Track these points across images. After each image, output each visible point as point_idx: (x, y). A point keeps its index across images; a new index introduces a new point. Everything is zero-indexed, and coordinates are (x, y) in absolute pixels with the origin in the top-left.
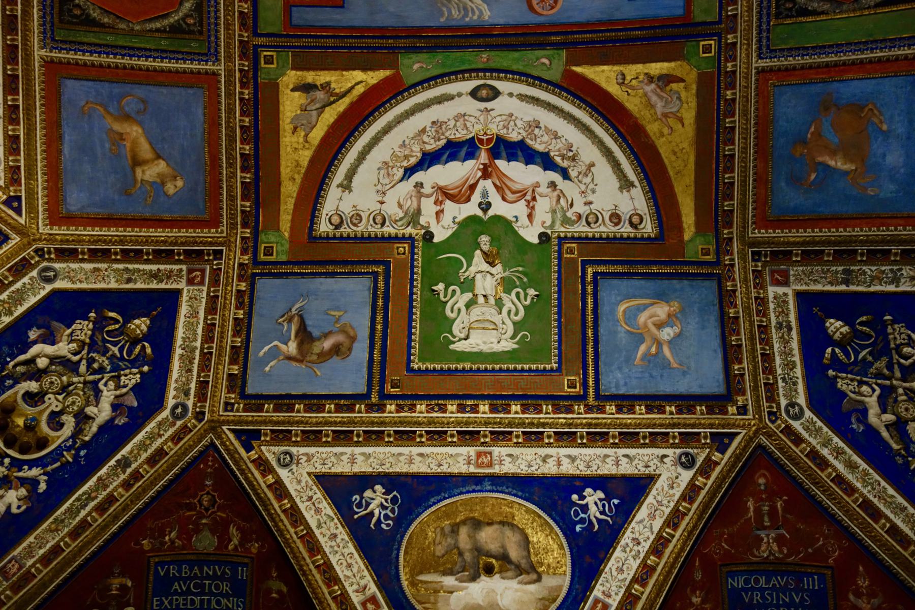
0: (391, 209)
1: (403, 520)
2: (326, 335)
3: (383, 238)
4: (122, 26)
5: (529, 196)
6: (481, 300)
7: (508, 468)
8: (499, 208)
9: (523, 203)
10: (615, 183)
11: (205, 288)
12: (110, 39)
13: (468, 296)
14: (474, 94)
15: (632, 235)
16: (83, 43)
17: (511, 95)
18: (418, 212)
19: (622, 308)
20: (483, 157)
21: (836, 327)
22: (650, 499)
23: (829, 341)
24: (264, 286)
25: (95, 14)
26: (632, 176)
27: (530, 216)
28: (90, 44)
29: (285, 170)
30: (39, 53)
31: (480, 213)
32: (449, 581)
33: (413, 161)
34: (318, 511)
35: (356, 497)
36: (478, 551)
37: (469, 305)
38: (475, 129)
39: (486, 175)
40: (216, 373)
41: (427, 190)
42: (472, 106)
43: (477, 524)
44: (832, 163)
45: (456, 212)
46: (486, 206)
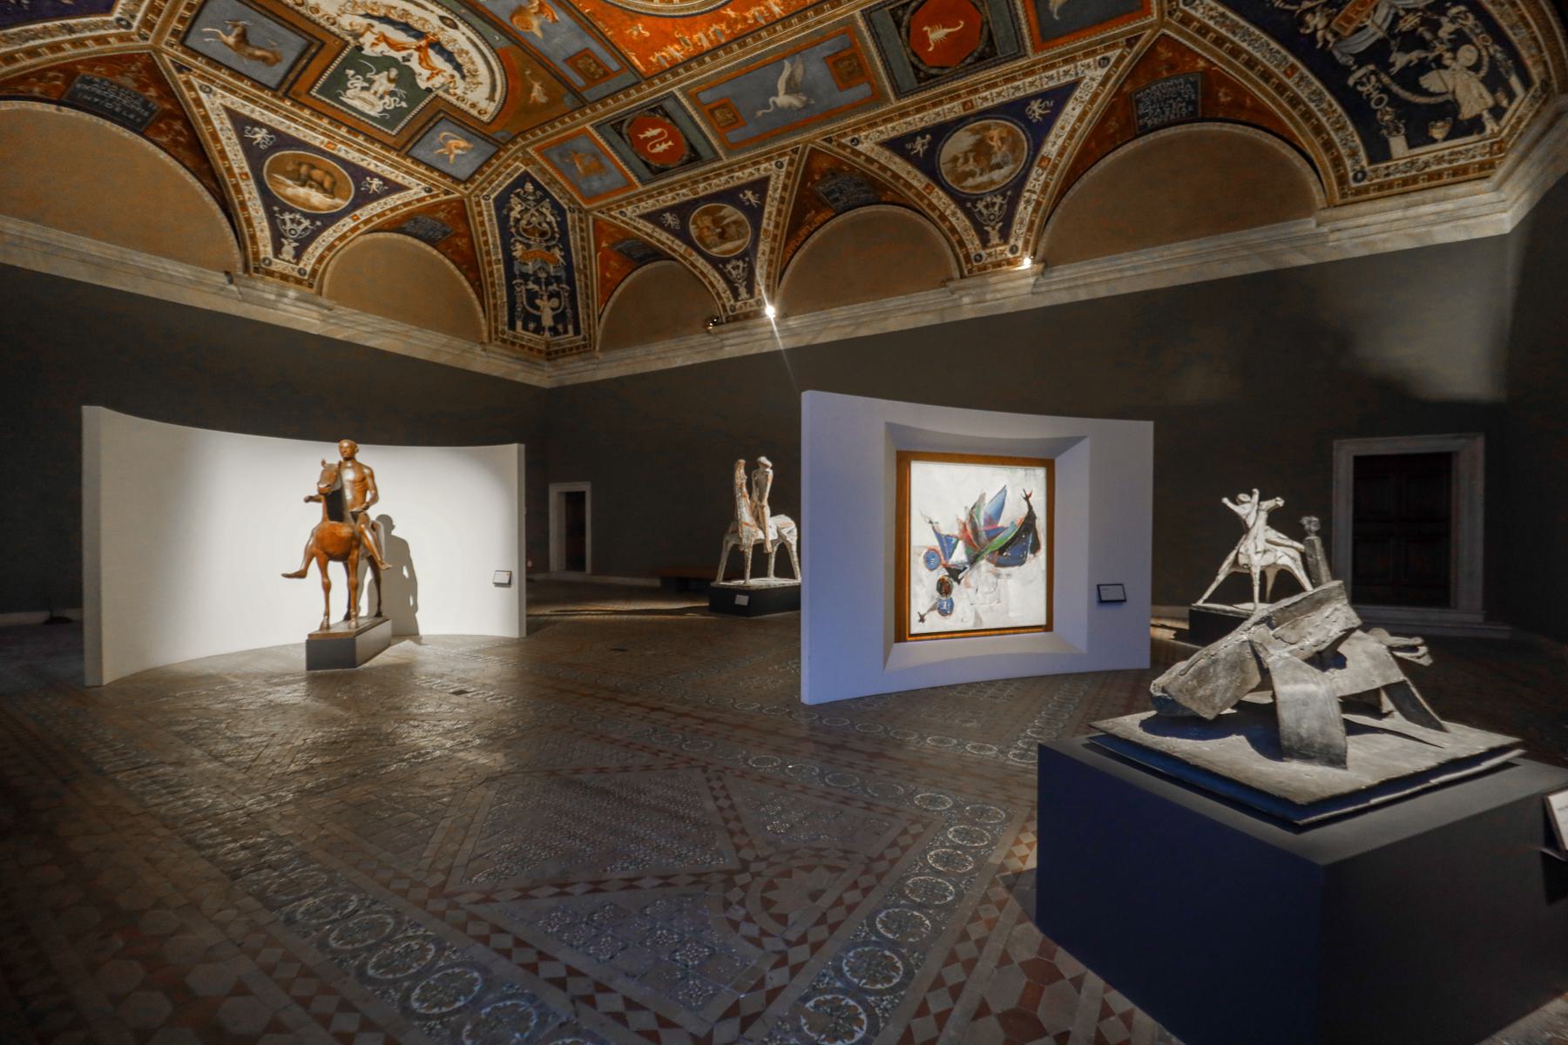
3: (328, 31)
5: (435, 72)
6: (372, 91)
7: (342, 154)
8: (414, 64)
9: (430, 72)
10: (487, 95)
13: (366, 84)
14: (442, 18)
18: (362, 35)
19: (445, 134)
20: (423, 43)
21: (529, 187)
22: (402, 194)
26: (498, 96)
27: (428, 79)
31: (400, 60)
32: (289, 182)
33: (375, 14)
35: (249, 128)
37: (363, 89)
39: (419, 49)
41: (375, 30)
42: (437, 22)
44: (578, 165)
45: (383, 48)
46: (406, 59)
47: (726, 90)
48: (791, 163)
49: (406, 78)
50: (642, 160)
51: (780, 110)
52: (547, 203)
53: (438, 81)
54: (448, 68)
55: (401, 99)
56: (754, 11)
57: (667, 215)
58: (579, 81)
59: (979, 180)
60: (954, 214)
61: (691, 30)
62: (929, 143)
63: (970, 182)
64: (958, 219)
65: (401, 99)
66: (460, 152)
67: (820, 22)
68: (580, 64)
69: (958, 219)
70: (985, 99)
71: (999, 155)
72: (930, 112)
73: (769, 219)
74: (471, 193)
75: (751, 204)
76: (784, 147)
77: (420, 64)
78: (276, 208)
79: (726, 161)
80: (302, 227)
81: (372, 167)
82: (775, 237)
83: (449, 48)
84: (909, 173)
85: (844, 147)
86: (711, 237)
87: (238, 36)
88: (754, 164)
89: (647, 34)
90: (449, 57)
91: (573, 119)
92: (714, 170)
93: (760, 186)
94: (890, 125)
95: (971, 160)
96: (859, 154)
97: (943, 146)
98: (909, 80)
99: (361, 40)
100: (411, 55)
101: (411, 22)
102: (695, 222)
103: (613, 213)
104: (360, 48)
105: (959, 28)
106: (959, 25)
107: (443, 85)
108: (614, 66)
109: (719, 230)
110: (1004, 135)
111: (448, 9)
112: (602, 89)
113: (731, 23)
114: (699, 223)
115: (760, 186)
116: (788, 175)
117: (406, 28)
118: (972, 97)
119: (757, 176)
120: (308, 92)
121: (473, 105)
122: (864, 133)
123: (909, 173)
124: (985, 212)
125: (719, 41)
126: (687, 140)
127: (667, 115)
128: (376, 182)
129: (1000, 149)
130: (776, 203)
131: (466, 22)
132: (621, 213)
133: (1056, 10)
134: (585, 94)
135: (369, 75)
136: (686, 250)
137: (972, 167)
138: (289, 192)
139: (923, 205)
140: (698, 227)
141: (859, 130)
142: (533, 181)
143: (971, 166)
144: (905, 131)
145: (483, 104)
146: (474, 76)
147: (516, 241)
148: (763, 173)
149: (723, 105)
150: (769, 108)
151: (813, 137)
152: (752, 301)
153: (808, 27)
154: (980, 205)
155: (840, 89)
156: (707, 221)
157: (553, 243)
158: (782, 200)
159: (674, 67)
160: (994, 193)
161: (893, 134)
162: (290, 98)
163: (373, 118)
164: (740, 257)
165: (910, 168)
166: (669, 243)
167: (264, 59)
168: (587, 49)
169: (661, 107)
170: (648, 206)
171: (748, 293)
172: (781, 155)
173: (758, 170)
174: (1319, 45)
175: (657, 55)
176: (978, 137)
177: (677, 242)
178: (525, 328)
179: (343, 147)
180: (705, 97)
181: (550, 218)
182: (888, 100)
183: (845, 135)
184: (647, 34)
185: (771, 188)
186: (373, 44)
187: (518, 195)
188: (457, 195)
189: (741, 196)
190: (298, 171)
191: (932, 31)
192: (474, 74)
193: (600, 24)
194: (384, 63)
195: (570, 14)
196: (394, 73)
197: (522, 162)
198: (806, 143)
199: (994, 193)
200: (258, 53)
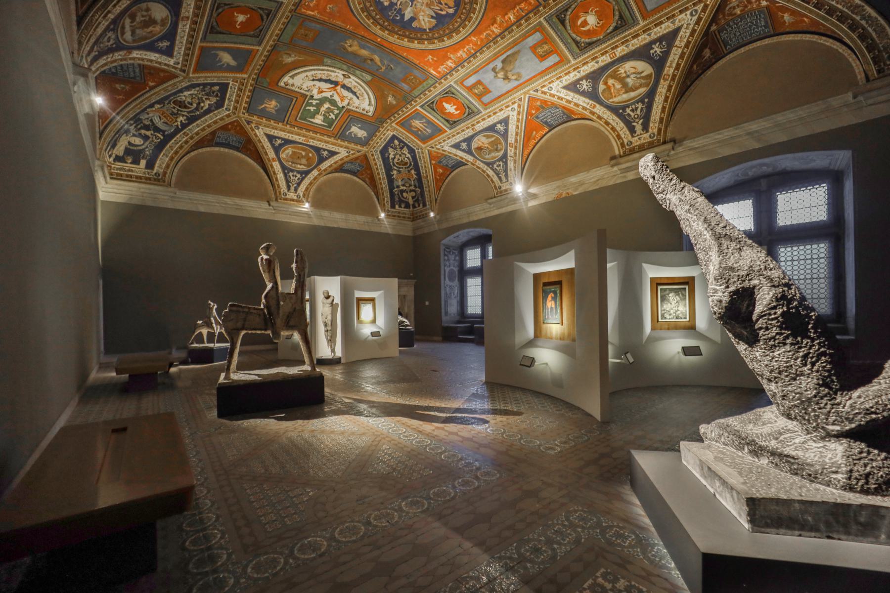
0: (304, 87)
4: (616, 8)
7: (311, 144)
10: (368, 103)
12: (624, 8)
14: (343, 75)
16: (630, 14)
21: (396, 142)
23: (393, 143)
25: (617, 17)
28: (629, 12)
30: (642, 23)
52: (405, 148)
54: (350, 95)
61: (456, 51)
78: (621, 111)
80: (297, 178)
90: (348, 89)
93: (505, 121)
100: (333, 94)
115: (505, 121)
124: (632, 114)
142: (398, 139)
145: (367, 108)
162: (289, 124)
164: (501, 159)
172: (513, 103)
174: (318, 102)
175: (442, 67)
178: (400, 206)
179: (311, 141)
181: (408, 155)
182: (570, 62)
187: (392, 147)
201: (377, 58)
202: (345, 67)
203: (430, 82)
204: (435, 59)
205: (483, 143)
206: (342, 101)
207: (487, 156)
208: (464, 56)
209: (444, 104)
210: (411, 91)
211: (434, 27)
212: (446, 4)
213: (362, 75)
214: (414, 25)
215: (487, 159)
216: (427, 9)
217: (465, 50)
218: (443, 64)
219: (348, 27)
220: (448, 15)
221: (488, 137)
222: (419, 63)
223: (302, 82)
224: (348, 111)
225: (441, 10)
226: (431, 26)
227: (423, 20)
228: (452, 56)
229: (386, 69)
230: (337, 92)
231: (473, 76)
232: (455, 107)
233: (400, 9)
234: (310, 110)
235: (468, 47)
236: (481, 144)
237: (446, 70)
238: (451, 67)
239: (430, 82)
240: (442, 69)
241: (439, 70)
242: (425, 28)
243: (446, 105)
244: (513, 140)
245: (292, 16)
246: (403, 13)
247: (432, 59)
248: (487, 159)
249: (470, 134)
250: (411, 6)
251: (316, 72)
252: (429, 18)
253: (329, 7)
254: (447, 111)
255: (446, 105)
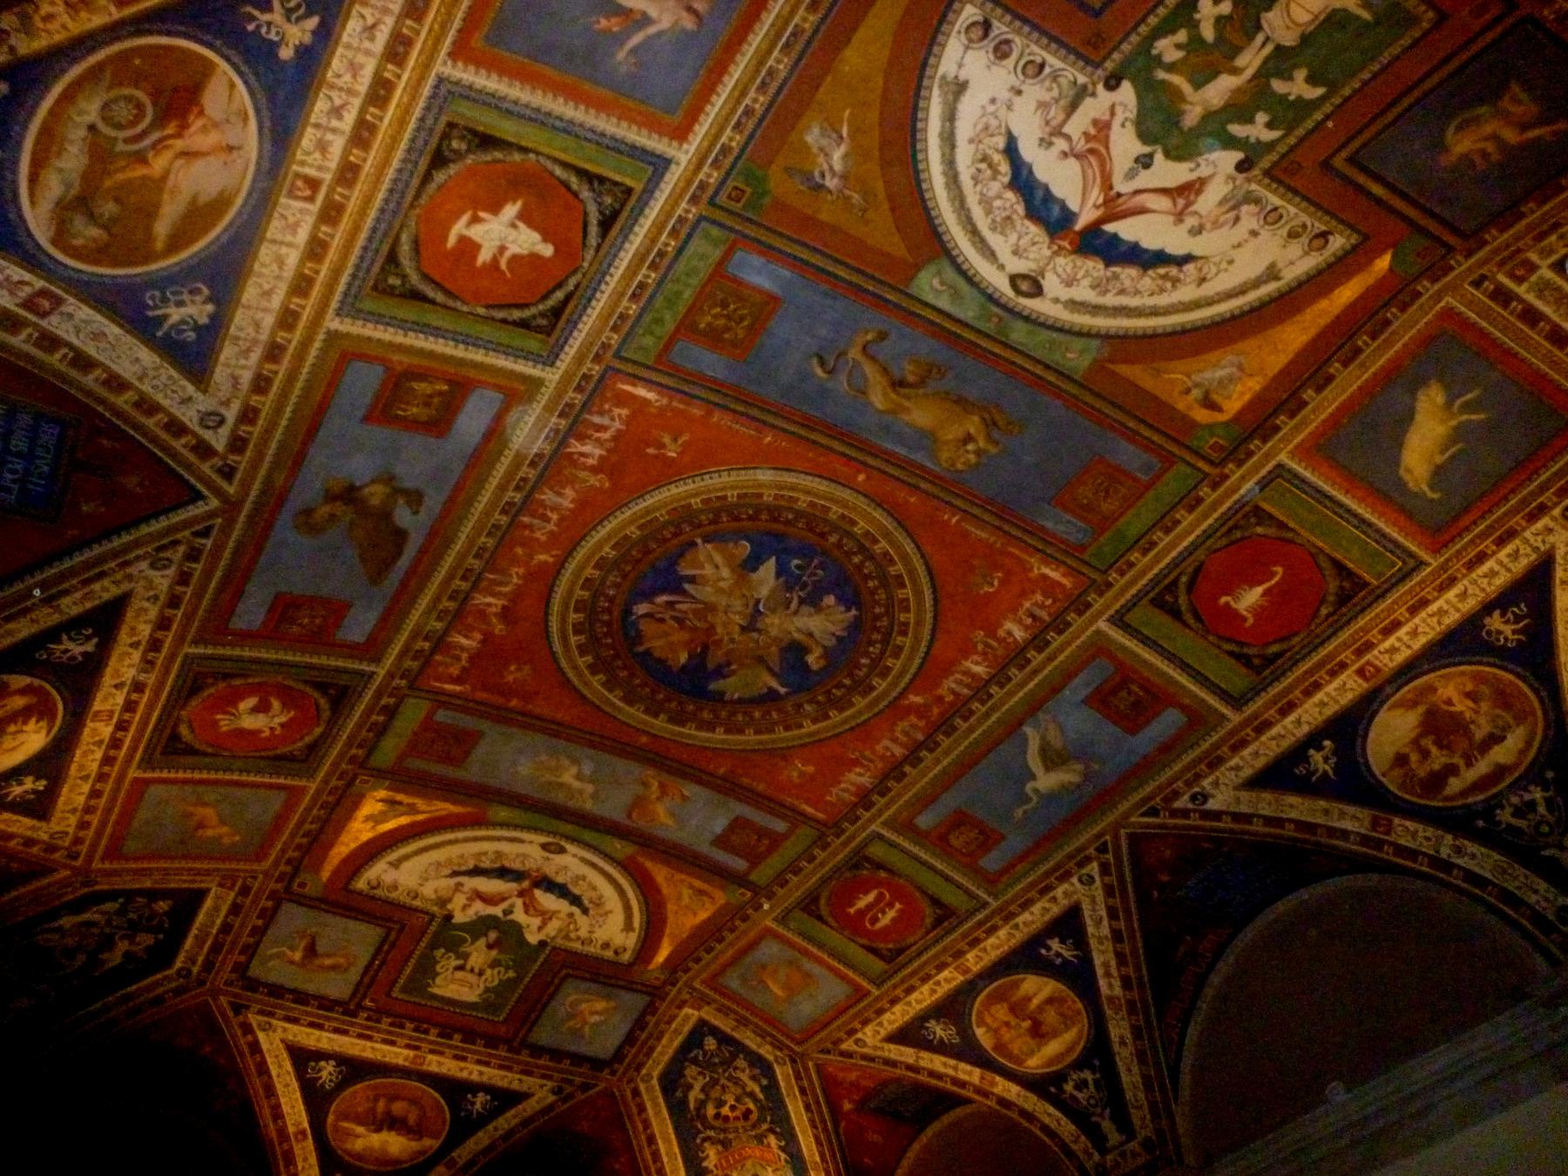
1: (341, 1086)
2: (329, 956)
5: (547, 916)
7: (434, 1068)
8: (519, 916)
11: (232, 894)
13: (461, 962)
14: (544, 847)
15: (999, 11)
17: (575, 856)
18: (450, 900)
20: (526, 884)
21: (710, 1043)
23: (701, 1046)
24: (288, 908)
27: (540, 929)
29: (344, 838)
32: (360, 1130)
33: (464, 868)
34: (280, 1066)
36: (388, 1113)
38: (530, 865)
39: (521, 894)
40: (224, 959)
43: (394, 1098)
45: (480, 908)
47: (950, 802)
48: (1105, 869)
49: (505, 934)
50: (863, 946)
51: (1050, 798)
53: (553, 928)
54: (563, 906)
55: (507, 968)
56: (950, 683)
57: (932, 1024)
58: (740, 864)
59: (1471, 775)
60: (1459, 851)
61: (583, 504)
62: (1335, 753)
63: (1454, 785)
64: (1473, 856)
65: (507, 968)
66: (596, 1018)
67: (1050, 659)
68: (736, 839)
69: (1473, 856)
70: (1393, 650)
71: (1482, 721)
72: (1306, 706)
73: (1108, 974)
74: (620, 1080)
75: (1065, 961)
76: (1080, 850)
77: (526, 912)
79: (994, 904)
81: (475, 1077)
82: (1131, 1005)
83: (560, 879)
84: (1326, 812)
85: (1185, 813)
86: (1018, 1041)
87: (305, 949)
88: (1043, 892)
89: (811, 769)
90: (562, 891)
91: (289, 862)
92: (980, 924)
94: (1246, 752)
95: (1434, 750)
96: (1217, 815)
97: (1364, 749)
98: (1238, 678)
99: (449, 906)
101: (507, 864)
102: (981, 1023)
103: (844, 1046)
104: (449, 917)
105: (1276, 579)
106: (1273, 574)
107: (560, 930)
108: (780, 826)
109: (1027, 1024)
110: (1469, 687)
111: (549, 833)
112: (775, 863)
113: (921, 711)
114: (989, 1020)
116: (1109, 891)
117: (503, 873)
118: (1368, 657)
119: (1055, 910)
120: (388, 994)
121: (606, 945)
122: (1210, 780)
123: (1326, 812)
125: (915, 741)
126: (924, 892)
127: (880, 866)
128: (481, 1098)
129: (1476, 712)
130: (1109, 946)
131: (573, 840)
132: (857, 1042)
133: (1425, 488)
134: (753, 877)
135: (462, 949)
136: (982, 1078)
137: (1444, 760)
138: (358, 1145)
139: (1387, 854)
140: (989, 1029)
141: (1198, 777)
142: (715, 1031)
143: (1438, 759)
144: (1278, 751)
146: (598, 905)
147: (704, 1140)
148: (1065, 902)
149: (960, 820)
150: (1028, 800)
151: (1128, 811)
152: (1133, 1145)
153: (1035, 672)
154: (1505, 816)
155: (1133, 730)
156: (1001, 1012)
157: (765, 1126)
158: (1117, 936)
159: (864, 799)
160: (1518, 785)
161: (1260, 763)
163: (472, 1006)
165: (1322, 803)
166: (951, 1072)
167: (333, 968)
168: (736, 819)
169: (867, 859)
170: (896, 1017)
171: (1119, 1130)
173: (1054, 899)
175: (834, 791)
176: (1421, 709)
177: (962, 1065)
180: (925, 821)
183: (1176, 795)
184: (811, 769)
185: (1089, 921)
186: (465, 908)
187: (695, 1061)
188: (602, 1086)
189: (1043, 951)
190: (373, 1110)
191: (1236, 599)
192: (599, 903)
193: (745, 781)
194: (480, 926)
195: (700, 782)
196: (493, 935)
197: (693, 1007)
198: (1115, 828)
199: (1518, 785)
200: (328, 962)
201: (879, 398)
202: (1019, 333)
203: (648, 341)
204: (651, 451)
205: (187, 154)
206: (1102, 129)
207: (89, 109)
208: (548, 496)
209: (547, 251)
210: (728, 254)
211: (681, 555)
212: (662, 620)
213: (956, 295)
214: (745, 548)
215: (68, 97)
216: (713, 599)
217: (555, 517)
218: (615, 438)
219: (954, 520)
220: (648, 595)
221: (199, 215)
222: (709, 413)
223: (1237, 255)
224: (1088, 51)
225: (671, 604)
226: (688, 557)
227: (717, 567)
228: (594, 480)
229: (842, 354)
230: (1107, 185)
231: (477, 439)
232: (484, 256)
233: (790, 589)
234: (1312, 80)
235: (551, 527)
236: (198, 137)
237: (597, 419)
238: (582, 438)
239: (648, 341)
240: (613, 420)
241: (625, 412)
242: (709, 546)
243: (527, 241)
244: (64, 331)
245: (1105, 572)
246: (782, 580)
247: (662, 446)
248: (68, 97)
249: (308, 138)
250: (758, 601)
251: (1163, 300)
252: (703, 576)
253: (992, 585)
254: (511, 210)
255: (527, 241)
